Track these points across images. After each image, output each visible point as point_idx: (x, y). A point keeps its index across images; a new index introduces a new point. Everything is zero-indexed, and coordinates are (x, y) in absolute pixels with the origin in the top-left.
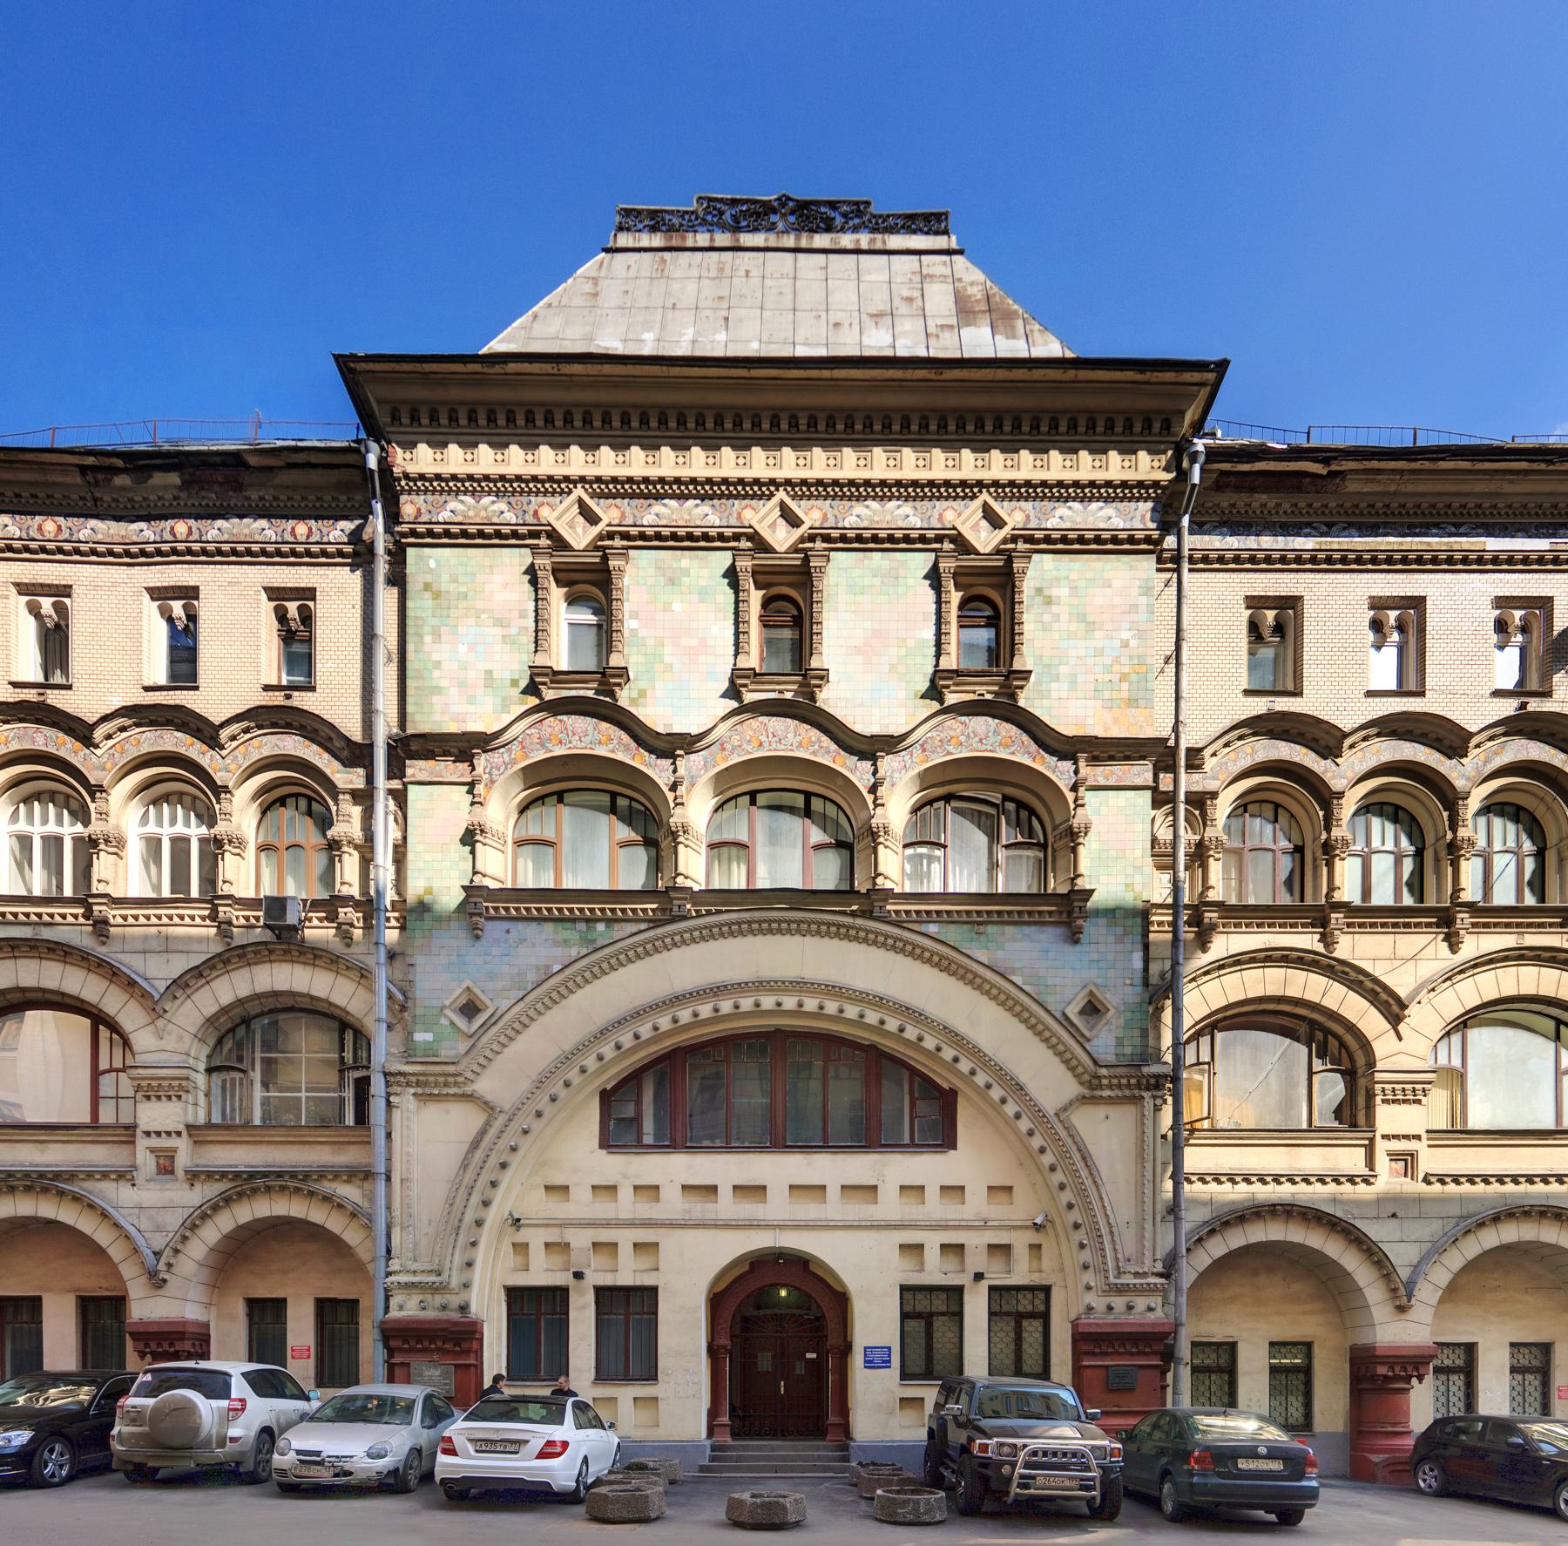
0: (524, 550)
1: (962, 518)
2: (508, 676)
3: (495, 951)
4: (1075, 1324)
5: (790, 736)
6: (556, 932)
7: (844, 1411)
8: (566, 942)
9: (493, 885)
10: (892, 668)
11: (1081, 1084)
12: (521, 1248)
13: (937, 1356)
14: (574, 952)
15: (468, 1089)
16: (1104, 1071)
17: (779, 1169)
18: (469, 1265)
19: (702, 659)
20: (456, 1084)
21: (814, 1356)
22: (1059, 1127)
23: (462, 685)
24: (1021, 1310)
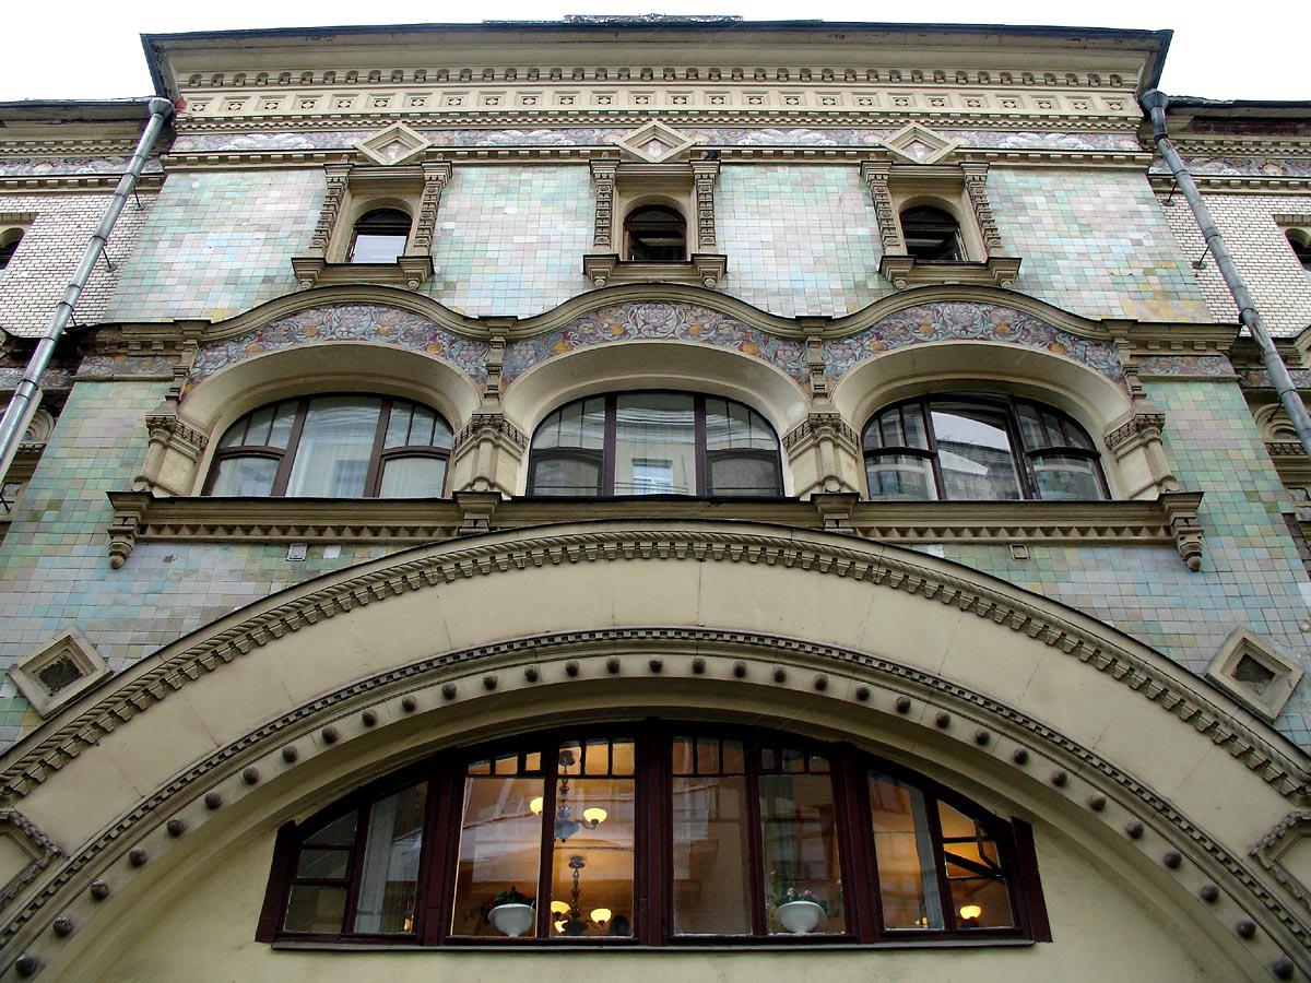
5: (671, 323)
6: (252, 561)
10: (817, 261)
11: (1288, 796)
13: (1165, 388)
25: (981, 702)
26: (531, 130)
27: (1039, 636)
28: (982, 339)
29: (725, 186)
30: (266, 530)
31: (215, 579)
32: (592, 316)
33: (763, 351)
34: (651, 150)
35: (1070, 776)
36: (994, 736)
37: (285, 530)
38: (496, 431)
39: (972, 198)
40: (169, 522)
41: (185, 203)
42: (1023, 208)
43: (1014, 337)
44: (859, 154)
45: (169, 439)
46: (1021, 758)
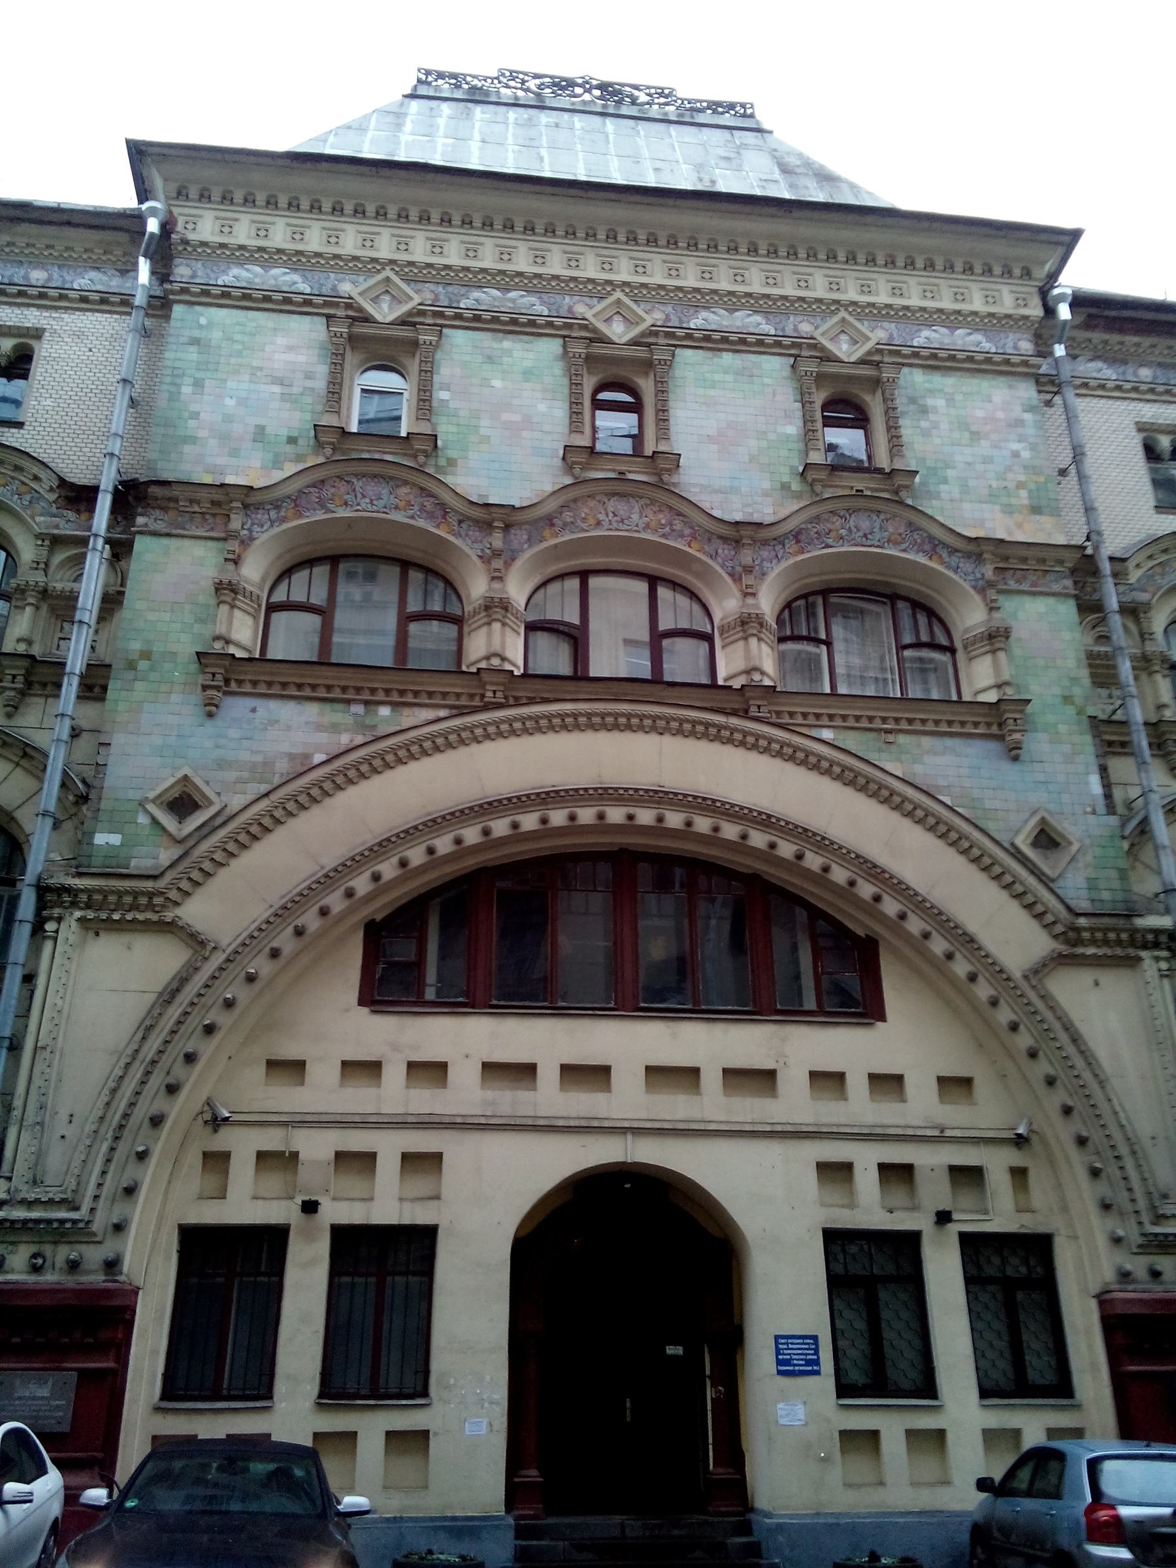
0: (316, 319)
1: (820, 330)
2: (284, 433)
3: (233, 733)
4: (1103, 1300)
5: (635, 517)
7: (733, 1452)
8: (335, 728)
9: (239, 654)
10: (752, 459)
11: (1055, 937)
12: (217, 1161)
14: (345, 740)
15: (169, 916)
16: (1082, 921)
17: (630, 1043)
18: (130, 1191)
19: (525, 434)
20: (150, 907)
21: (679, 1350)
22: (1032, 995)
23: (224, 437)
24: (1012, 1274)
25: (853, 856)
26: (509, 290)
27: (897, 808)
28: (878, 547)
29: (677, 359)
30: (329, 688)
31: (295, 730)
32: (572, 505)
33: (706, 547)
34: (615, 325)
35: (909, 913)
36: (860, 881)
37: (344, 689)
38: (503, 612)
39: (885, 400)
40: (248, 677)
41: (195, 342)
42: (924, 411)
43: (904, 546)
44: (794, 345)
45: (234, 599)
46: (877, 899)
